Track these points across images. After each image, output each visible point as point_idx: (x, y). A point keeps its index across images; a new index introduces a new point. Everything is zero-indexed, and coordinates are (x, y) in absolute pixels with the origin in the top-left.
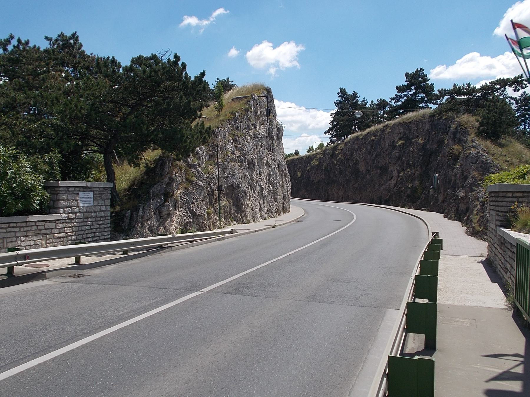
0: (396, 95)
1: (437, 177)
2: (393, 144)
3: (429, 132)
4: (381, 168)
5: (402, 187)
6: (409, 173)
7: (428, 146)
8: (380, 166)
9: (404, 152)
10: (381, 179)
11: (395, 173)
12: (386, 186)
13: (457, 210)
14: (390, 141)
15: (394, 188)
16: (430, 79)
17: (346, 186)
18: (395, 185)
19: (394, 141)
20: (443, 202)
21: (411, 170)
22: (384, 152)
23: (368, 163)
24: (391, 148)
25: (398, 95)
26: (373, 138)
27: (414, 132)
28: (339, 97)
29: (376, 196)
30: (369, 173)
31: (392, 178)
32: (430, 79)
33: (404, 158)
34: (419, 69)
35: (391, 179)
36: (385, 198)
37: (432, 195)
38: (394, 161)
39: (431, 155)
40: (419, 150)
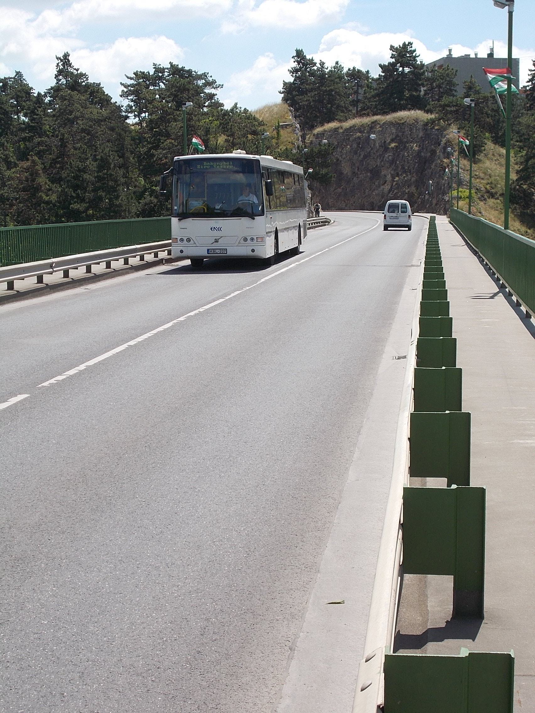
0: (379, 75)
1: (431, 184)
2: (384, 145)
3: (423, 141)
4: (371, 171)
5: (398, 193)
6: (406, 178)
7: (423, 154)
8: (369, 168)
9: (398, 155)
10: (373, 183)
11: (389, 177)
12: (379, 191)
13: (445, 208)
14: (381, 142)
15: (389, 193)
16: (419, 55)
17: (323, 191)
18: (390, 191)
19: (385, 142)
20: (436, 204)
21: (407, 175)
22: (374, 154)
23: (354, 164)
24: (383, 149)
25: (382, 75)
26: (359, 134)
27: (408, 136)
28: (294, 62)
29: (367, 202)
30: (357, 176)
31: (385, 183)
32: (419, 55)
33: (398, 162)
34: (407, 43)
35: (384, 184)
36: (379, 204)
37: (427, 199)
38: (387, 165)
39: (425, 163)
40: (415, 157)
